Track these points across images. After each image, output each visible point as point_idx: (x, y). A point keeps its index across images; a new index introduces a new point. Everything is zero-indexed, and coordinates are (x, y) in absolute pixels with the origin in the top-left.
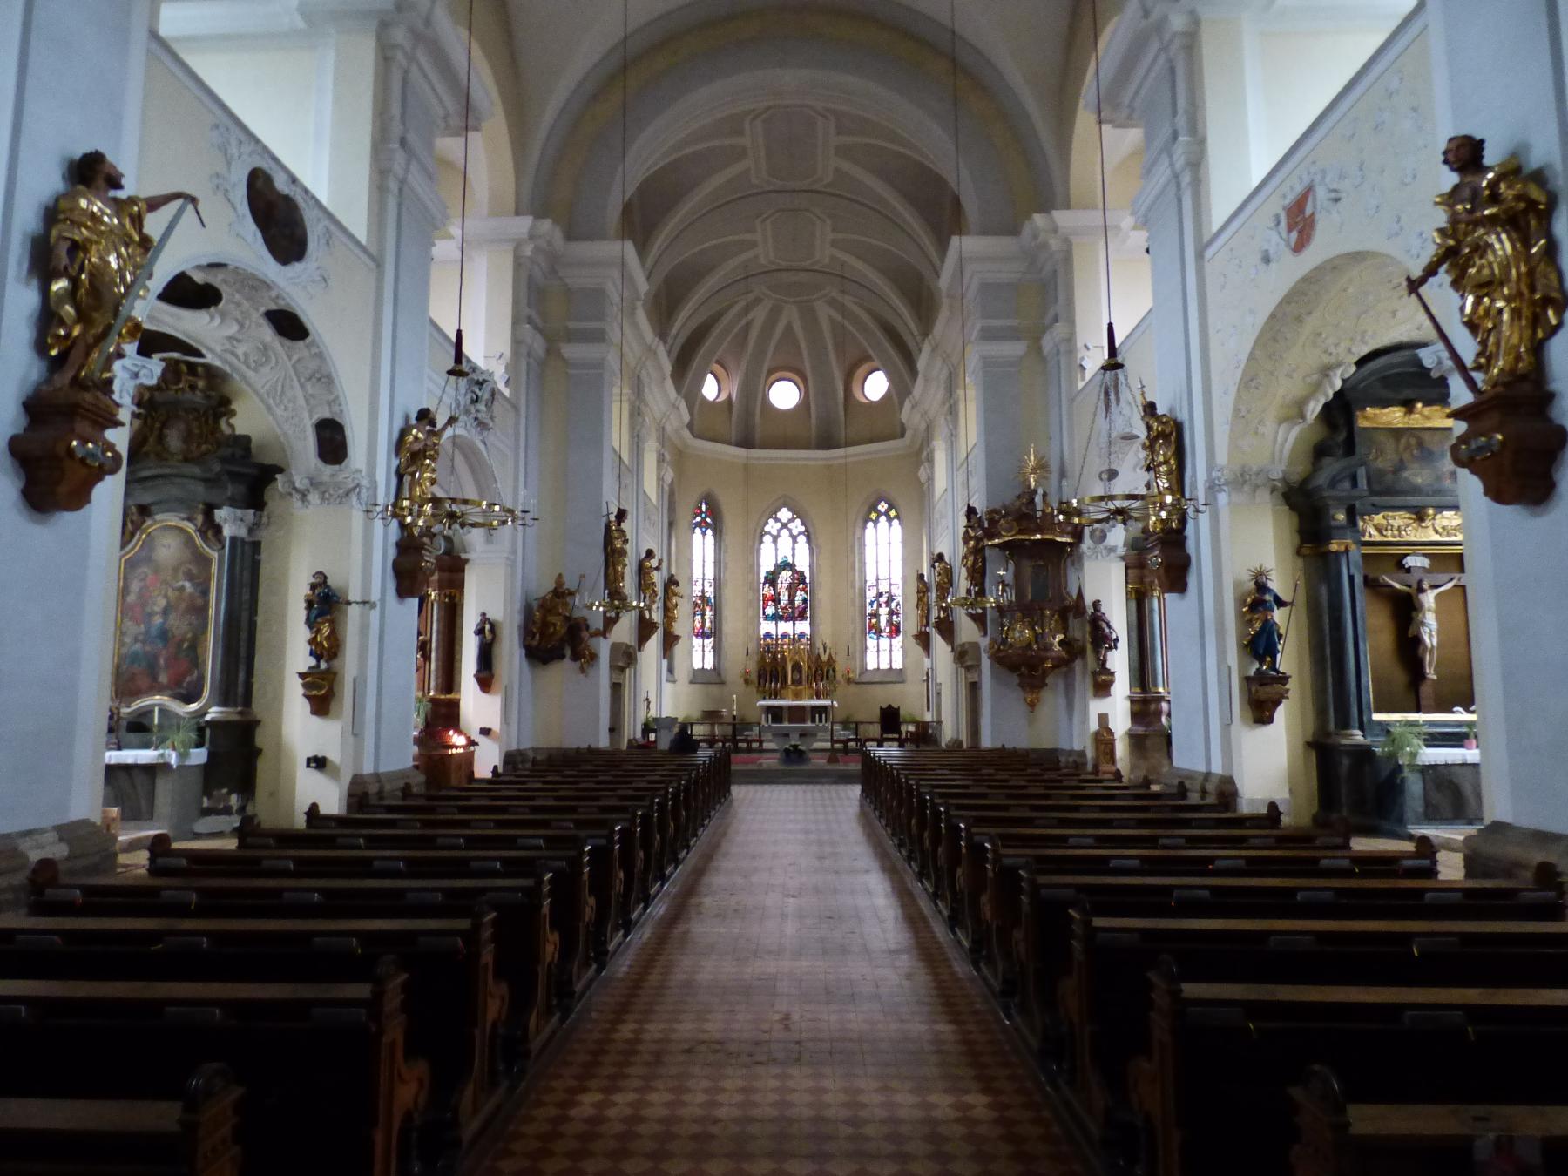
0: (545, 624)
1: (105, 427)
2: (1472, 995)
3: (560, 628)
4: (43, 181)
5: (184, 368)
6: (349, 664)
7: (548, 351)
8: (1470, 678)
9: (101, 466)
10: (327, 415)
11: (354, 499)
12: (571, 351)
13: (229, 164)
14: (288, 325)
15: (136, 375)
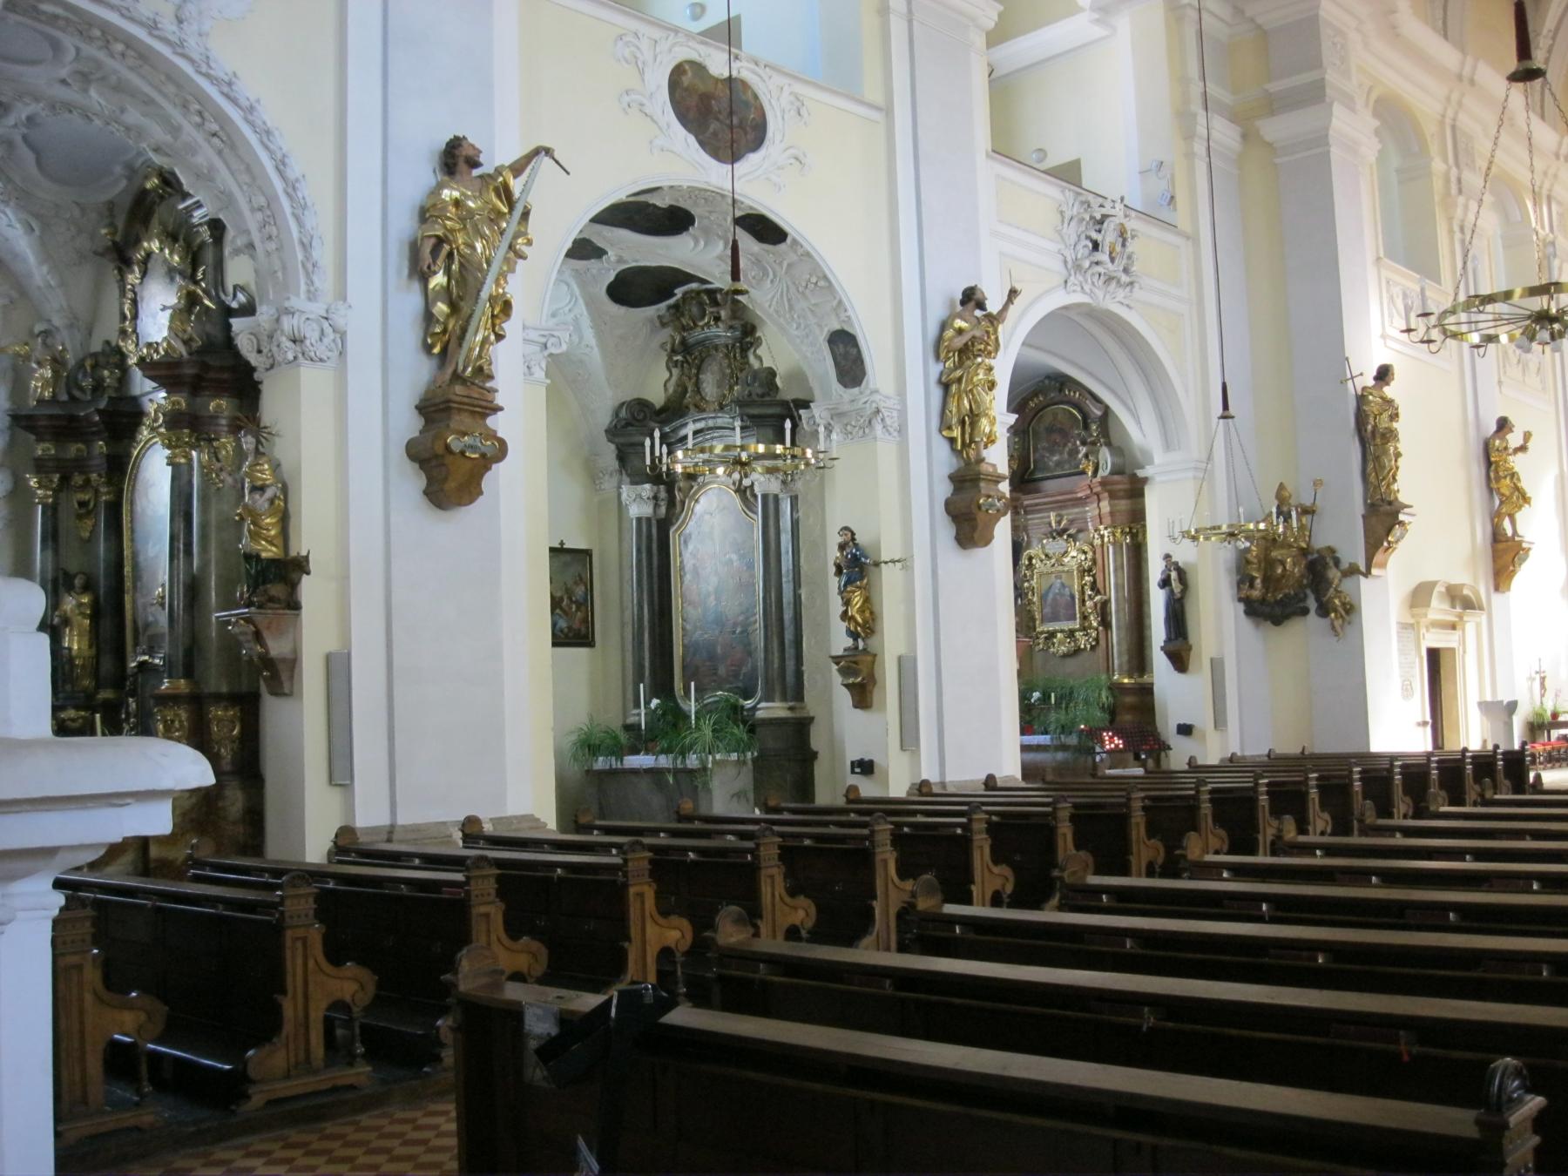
0: (1268, 563)
1: (484, 416)
3: (1291, 565)
4: (418, 176)
6: (890, 644)
7: (1244, 136)
8: (349, 655)
10: (837, 327)
11: (878, 427)
12: (1274, 129)
13: (642, 73)
14: (765, 230)
15: (545, 346)
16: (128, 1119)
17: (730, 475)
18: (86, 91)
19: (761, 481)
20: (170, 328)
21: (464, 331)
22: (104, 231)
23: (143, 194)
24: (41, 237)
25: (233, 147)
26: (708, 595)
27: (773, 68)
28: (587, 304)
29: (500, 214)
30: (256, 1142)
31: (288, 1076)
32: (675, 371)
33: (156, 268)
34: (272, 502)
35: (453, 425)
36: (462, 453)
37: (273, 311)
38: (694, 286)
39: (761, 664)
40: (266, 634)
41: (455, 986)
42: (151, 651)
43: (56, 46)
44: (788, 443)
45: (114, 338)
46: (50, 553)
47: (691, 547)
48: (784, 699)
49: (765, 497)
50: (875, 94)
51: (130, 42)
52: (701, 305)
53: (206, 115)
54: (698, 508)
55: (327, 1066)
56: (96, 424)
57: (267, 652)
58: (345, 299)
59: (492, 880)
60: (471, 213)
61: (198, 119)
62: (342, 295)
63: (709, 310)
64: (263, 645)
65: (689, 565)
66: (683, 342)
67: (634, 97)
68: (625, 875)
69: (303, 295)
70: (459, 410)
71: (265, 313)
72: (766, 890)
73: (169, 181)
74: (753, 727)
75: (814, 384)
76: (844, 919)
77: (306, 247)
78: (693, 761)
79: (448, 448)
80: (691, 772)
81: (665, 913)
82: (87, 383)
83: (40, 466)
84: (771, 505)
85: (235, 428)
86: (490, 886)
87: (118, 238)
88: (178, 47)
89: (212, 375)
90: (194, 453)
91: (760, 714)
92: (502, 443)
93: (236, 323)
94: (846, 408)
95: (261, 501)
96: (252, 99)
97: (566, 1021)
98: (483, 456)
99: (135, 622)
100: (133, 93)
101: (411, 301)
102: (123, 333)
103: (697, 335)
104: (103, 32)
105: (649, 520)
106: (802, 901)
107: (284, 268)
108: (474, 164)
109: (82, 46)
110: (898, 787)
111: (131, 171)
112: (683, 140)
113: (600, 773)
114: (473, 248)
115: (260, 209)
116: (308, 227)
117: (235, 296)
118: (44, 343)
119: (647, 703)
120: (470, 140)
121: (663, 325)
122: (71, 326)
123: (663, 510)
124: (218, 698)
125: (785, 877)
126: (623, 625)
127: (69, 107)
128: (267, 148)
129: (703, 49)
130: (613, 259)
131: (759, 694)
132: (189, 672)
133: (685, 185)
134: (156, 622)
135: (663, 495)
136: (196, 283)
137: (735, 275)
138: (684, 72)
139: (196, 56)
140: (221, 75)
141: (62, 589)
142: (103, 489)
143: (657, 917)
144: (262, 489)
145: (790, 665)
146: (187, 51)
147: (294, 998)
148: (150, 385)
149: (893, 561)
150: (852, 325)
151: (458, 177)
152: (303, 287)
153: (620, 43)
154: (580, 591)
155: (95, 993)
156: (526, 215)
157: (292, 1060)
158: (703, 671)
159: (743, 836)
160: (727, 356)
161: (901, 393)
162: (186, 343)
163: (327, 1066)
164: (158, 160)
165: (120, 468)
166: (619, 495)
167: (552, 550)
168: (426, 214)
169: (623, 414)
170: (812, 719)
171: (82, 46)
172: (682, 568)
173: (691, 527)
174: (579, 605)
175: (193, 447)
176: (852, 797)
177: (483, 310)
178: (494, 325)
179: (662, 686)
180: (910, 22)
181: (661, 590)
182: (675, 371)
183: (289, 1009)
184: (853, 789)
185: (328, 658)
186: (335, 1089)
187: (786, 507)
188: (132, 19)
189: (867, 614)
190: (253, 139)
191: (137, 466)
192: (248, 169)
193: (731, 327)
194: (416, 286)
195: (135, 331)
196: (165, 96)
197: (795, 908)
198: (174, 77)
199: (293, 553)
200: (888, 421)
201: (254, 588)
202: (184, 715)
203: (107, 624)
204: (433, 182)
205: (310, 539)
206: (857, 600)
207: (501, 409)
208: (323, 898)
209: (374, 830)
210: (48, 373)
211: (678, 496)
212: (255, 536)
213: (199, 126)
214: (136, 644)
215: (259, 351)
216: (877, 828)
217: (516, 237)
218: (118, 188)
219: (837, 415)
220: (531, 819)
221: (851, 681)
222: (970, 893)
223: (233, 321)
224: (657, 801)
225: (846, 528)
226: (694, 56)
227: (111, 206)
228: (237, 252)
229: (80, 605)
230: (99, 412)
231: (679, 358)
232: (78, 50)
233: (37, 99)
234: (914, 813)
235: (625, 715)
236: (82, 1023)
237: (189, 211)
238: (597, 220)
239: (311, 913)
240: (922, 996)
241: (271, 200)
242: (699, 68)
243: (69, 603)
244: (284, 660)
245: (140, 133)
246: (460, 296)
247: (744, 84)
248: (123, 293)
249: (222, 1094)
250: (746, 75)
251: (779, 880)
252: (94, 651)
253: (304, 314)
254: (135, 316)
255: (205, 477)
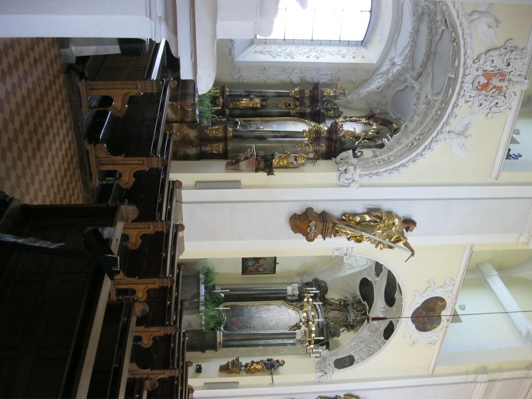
1: (322, 234)
2: (76, 332)
4: (402, 210)
5: (363, 312)
6: (243, 379)
8: (240, 188)
9: (308, 233)
10: (356, 358)
11: (320, 374)
13: (441, 287)
14: (389, 332)
15: (346, 255)
16: (85, 104)
17: (304, 318)
18: (424, 104)
19: (299, 334)
20: (348, 131)
21: (351, 227)
22: (378, 111)
23: (391, 123)
24: (375, 92)
25: (409, 150)
26: (260, 314)
27: (445, 334)
28: (360, 271)
29: (390, 239)
30: (74, 146)
31: (96, 157)
32: (338, 302)
33: (367, 128)
34: (292, 163)
35: (318, 223)
36: (309, 226)
37: (355, 163)
38: (368, 308)
39: (236, 333)
40: (247, 161)
41: (123, 204)
42: (241, 125)
43: (438, 94)
44: (315, 338)
45: (344, 115)
46: (274, 94)
47: (277, 308)
48: (224, 341)
49: (295, 334)
50: (438, 370)
51: (441, 116)
52: (361, 311)
53: (419, 141)
54: (290, 310)
55: (99, 171)
56: (316, 109)
57: (241, 161)
58: (360, 187)
59: (162, 230)
60: (391, 229)
61: (417, 138)
62: (361, 186)
63: (360, 313)
64: (244, 160)
65: (270, 307)
66: (348, 305)
67: (433, 284)
68: (163, 278)
69: (361, 173)
70: (324, 225)
71: (354, 161)
72: (155, 329)
73: (396, 131)
74: (214, 330)
75: (335, 351)
76: (142, 358)
77: (377, 174)
78: (202, 308)
79: (311, 221)
80: (198, 307)
81: (148, 292)
82: (329, 106)
83: (302, 92)
84: (292, 336)
85: (316, 152)
86: (160, 229)
87: (376, 115)
88: (441, 132)
89: (333, 144)
90: (307, 139)
91: (218, 332)
92: (313, 240)
93: (351, 152)
94: (327, 362)
95: (292, 160)
96: (425, 156)
97: (108, 241)
98: (308, 233)
99: (251, 121)
100: (424, 118)
101: (359, 208)
102: (346, 117)
103: (350, 308)
104: (444, 108)
105: (286, 293)
106: (151, 342)
107: (369, 167)
108: (407, 229)
109: (439, 102)
110: (192, 382)
111: (398, 119)
112: (418, 302)
113: (199, 276)
114: (379, 230)
115: (389, 159)
116: (384, 174)
117: (359, 152)
118: (341, 93)
119: (223, 293)
120: (415, 228)
121: (354, 298)
122: (347, 101)
123: (289, 298)
124: (226, 146)
125: (160, 337)
126: (250, 284)
127: (418, 99)
128: (409, 161)
129: (450, 308)
130: (376, 279)
131: (225, 332)
132: (234, 137)
133: (403, 303)
134: (251, 127)
135: (295, 298)
136: (363, 140)
137: (374, 319)
138: (442, 302)
139: (438, 137)
140: (432, 145)
141: (262, 98)
142: (294, 111)
143: (147, 289)
144: (296, 160)
145: (236, 343)
146: (439, 134)
147: (123, 160)
148: (329, 125)
149: (272, 380)
150: (356, 364)
151: (403, 224)
152: (363, 173)
153: (451, 279)
154: (261, 270)
155: (128, 93)
156: (391, 247)
157: (102, 159)
158: (233, 312)
159: (175, 322)
160: (343, 320)
161: (333, 382)
162: (343, 136)
163: (99, 171)
164: (403, 127)
165: (301, 116)
166: (295, 283)
167: (275, 258)
168: (390, 214)
169: (322, 284)
170: (216, 350)
171: (439, 102)
172: (269, 305)
173: (284, 308)
174: (256, 269)
175: (309, 138)
176: (188, 364)
177: (358, 233)
178: (353, 237)
179: (228, 298)
180: (464, 383)
181: (261, 297)
182: (338, 302)
183: (120, 158)
184: (191, 364)
185: (239, 181)
186: (91, 174)
187: (291, 341)
188: (448, 117)
189: (254, 370)
190: (412, 156)
191: (302, 122)
192: (401, 155)
193: (354, 321)
194: (365, 211)
195: (346, 121)
196: (424, 128)
197: (148, 340)
198: (430, 130)
199: (274, 170)
200: (322, 377)
201: (262, 157)
202: (220, 135)
203: (251, 112)
204: (400, 216)
205: (279, 176)
206: (258, 367)
207: (324, 239)
208: (158, 171)
209: (181, 197)
210: (332, 94)
211: (295, 303)
212: (280, 158)
213: (415, 139)
214: (244, 121)
215: (341, 159)
216: (177, 371)
217: (383, 244)
218: (392, 115)
219: (324, 359)
220: (183, 250)
221: (230, 365)
222: (141, 325)
223: (351, 151)
224: (188, 296)
225: (284, 363)
226: (448, 305)
227: (387, 113)
228: (374, 152)
229: (257, 104)
230: (320, 110)
231: (342, 303)
232: (437, 101)
233: (420, 89)
234: (182, 386)
235: (218, 285)
236: (117, 89)
237: (387, 137)
238: (389, 272)
239: (152, 167)
240: (111, 378)
241: (392, 162)
242: (444, 307)
243: (257, 100)
244: (238, 167)
245: (411, 121)
246: (362, 225)
247: (439, 323)
248: (358, 117)
249: (92, 135)
250: (442, 324)
251: (159, 334)
252: (241, 108)
253: (356, 174)
254: (351, 121)
255: (299, 142)
